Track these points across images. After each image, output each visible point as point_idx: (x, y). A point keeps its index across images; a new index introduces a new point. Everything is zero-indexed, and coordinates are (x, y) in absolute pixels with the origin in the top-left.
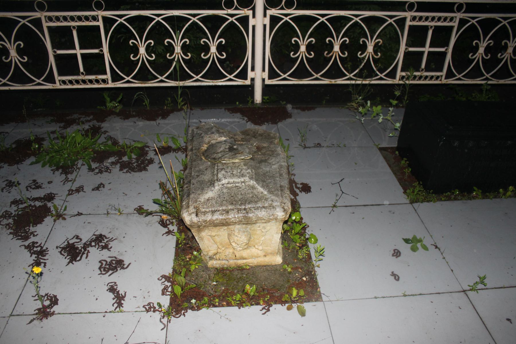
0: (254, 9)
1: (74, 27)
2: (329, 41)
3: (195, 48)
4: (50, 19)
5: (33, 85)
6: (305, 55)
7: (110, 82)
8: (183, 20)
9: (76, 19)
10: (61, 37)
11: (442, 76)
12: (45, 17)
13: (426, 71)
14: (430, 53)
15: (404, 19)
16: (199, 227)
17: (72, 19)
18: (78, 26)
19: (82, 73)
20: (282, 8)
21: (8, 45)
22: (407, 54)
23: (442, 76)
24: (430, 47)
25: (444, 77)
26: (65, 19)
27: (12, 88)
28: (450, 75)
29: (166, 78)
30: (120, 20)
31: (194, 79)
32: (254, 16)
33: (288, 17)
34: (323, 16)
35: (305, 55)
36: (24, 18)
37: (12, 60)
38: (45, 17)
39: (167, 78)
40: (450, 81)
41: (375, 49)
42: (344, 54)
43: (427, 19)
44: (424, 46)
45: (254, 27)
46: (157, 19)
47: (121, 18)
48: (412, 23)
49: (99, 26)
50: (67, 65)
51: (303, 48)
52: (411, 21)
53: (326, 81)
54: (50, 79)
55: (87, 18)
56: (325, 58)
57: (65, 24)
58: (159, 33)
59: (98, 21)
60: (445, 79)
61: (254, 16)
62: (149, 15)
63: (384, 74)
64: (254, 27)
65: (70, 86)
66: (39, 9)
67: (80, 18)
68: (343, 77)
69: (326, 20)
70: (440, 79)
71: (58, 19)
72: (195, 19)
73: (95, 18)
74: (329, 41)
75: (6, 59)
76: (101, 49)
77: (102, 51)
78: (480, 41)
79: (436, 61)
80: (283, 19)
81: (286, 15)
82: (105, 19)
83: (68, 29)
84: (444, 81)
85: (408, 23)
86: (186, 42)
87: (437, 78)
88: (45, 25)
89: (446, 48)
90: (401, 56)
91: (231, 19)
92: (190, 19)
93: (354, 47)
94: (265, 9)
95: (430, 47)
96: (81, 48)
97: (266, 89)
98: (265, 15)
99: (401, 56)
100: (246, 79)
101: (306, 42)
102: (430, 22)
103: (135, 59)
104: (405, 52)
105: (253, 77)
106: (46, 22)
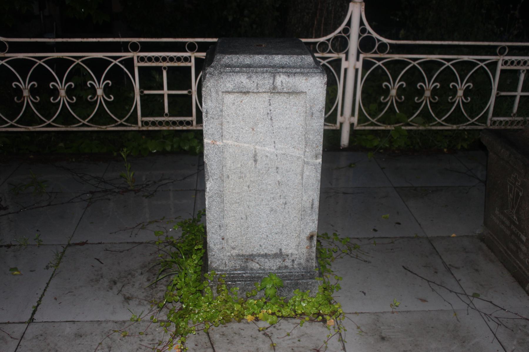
0: (347, 54)
1: (165, 68)
3: (80, 90)
4: (142, 59)
7: (194, 123)
10: (150, 77)
12: (138, 57)
15: (495, 63)
16: (325, 289)
17: (164, 59)
19: (166, 115)
20: (375, 53)
21: (59, 86)
24: (522, 91)
25: (194, 123)
26: (157, 59)
30: (77, 61)
31: (81, 124)
32: (347, 59)
34: (448, 60)
36: (115, 58)
38: (138, 57)
39: (17, 122)
41: (131, 95)
42: (73, 100)
43: (519, 63)
44: (515, 90)
45: (346, 70)
46: (77, 61)
48: (505, 67)
49: (190, 68)
50: (152, 105)
51: (460, 93)
52: (502, 65)
53: (449, 127)
54: (133, 119)
55: (179, 59)
56: (381, 103)
58: (42, 76)
59: (190, 62)
61: (347, 59)
62: (27, 58)
63: (124, 119)
64: (346, 70)
66: (320, 51)
67: (171, 59)
69: (452, 64)
71: (150, 59)
72: (116, 62)
73: (187, 59)
76: (190, 90)
77: (190, 92)
80: (75, 62)
81: (379, 59)
82: (197, 59)
85: (500, 67)
86: (108, 83)
88: (137, 64)
93: (444, 92)
94: (358, 53)
95: (522, 91)
96: (169, 89)
97: (353, 133)
98: (358, 59)
100: (335, 123)
101: (397, 86)
102: (515, 66)
103: (20, 101)
105: (342, 122)
106: (138, 62)
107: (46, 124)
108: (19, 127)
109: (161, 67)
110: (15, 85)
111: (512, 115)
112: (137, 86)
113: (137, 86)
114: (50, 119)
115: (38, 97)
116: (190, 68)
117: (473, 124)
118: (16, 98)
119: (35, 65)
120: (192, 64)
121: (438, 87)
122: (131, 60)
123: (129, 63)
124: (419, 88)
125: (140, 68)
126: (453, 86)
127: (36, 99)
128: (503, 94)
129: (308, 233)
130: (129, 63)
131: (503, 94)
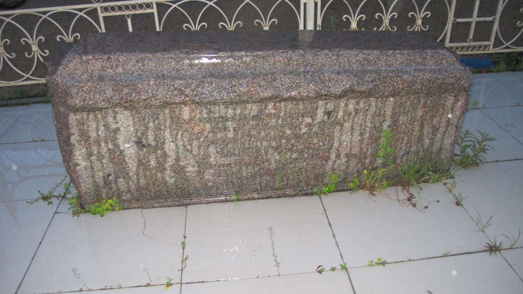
1: (128, 16)
2: (412, 15)
4: (106, 9)
5: (501, 49)
6: (41, 55)
8: (70, 16)
9: (130, 7)
11: (490, 45)
12: (101, 7)
13: (474, 41)
14: (477, 23)
18: (132, 15)
21: (30, 42)
22: (456, 25)
23: (490, 45)
25: (491, 47)
26: (120, 8)
27: (514, 50)
28: (498, 43)
29: (32, 75)
31: (24, 78)
33: (10, 18)
35: (41, 55)
37: (34, 55)
38: (101, 7)
40: (498, 50)
47: (8, 18)
49: (153, 14)
57: (119, 13)
59: (152, 8)
60: (494, 47)
65: (475, 52)
68: (501, 46)
70: (487, 49)
71: (113, 9)
72: (81, 14)
74: (412, 15)
75: (29, 54)
78: (416, 12)
79: (483, 32)
83: (123, 18)
84: (491, 50)
86: (77, 36)
87: (486, 46)
88: (101, 15)
89: (493, 17)
90: (449, 27)
91: (44, 17)
92: (41, 17)
95: (478, 17)
99: (449, 27)
104: (453, 24)
106: (102, 12)
107: (24, 78)
108: (513, 48)
109: (124, 16)
110: (24, 41)
111: (468, 40)
112: (496, 26)
113: (496, 26)
114: (29, 72)
115: (46, 51)
116: (153, 14)
117: (507, 47)
118: (26, 53)
119: (3, 23)
120: (155, 10)
121: (364, 19)
122: (95, 10)
123: (93, 13)
124: (345, 20)
125: (104, 18)
126: (379, 16)
127: (12, 56)
128: (459, 20)
129: (100, 218)
130: (93, 13)
131: (459, 20)
